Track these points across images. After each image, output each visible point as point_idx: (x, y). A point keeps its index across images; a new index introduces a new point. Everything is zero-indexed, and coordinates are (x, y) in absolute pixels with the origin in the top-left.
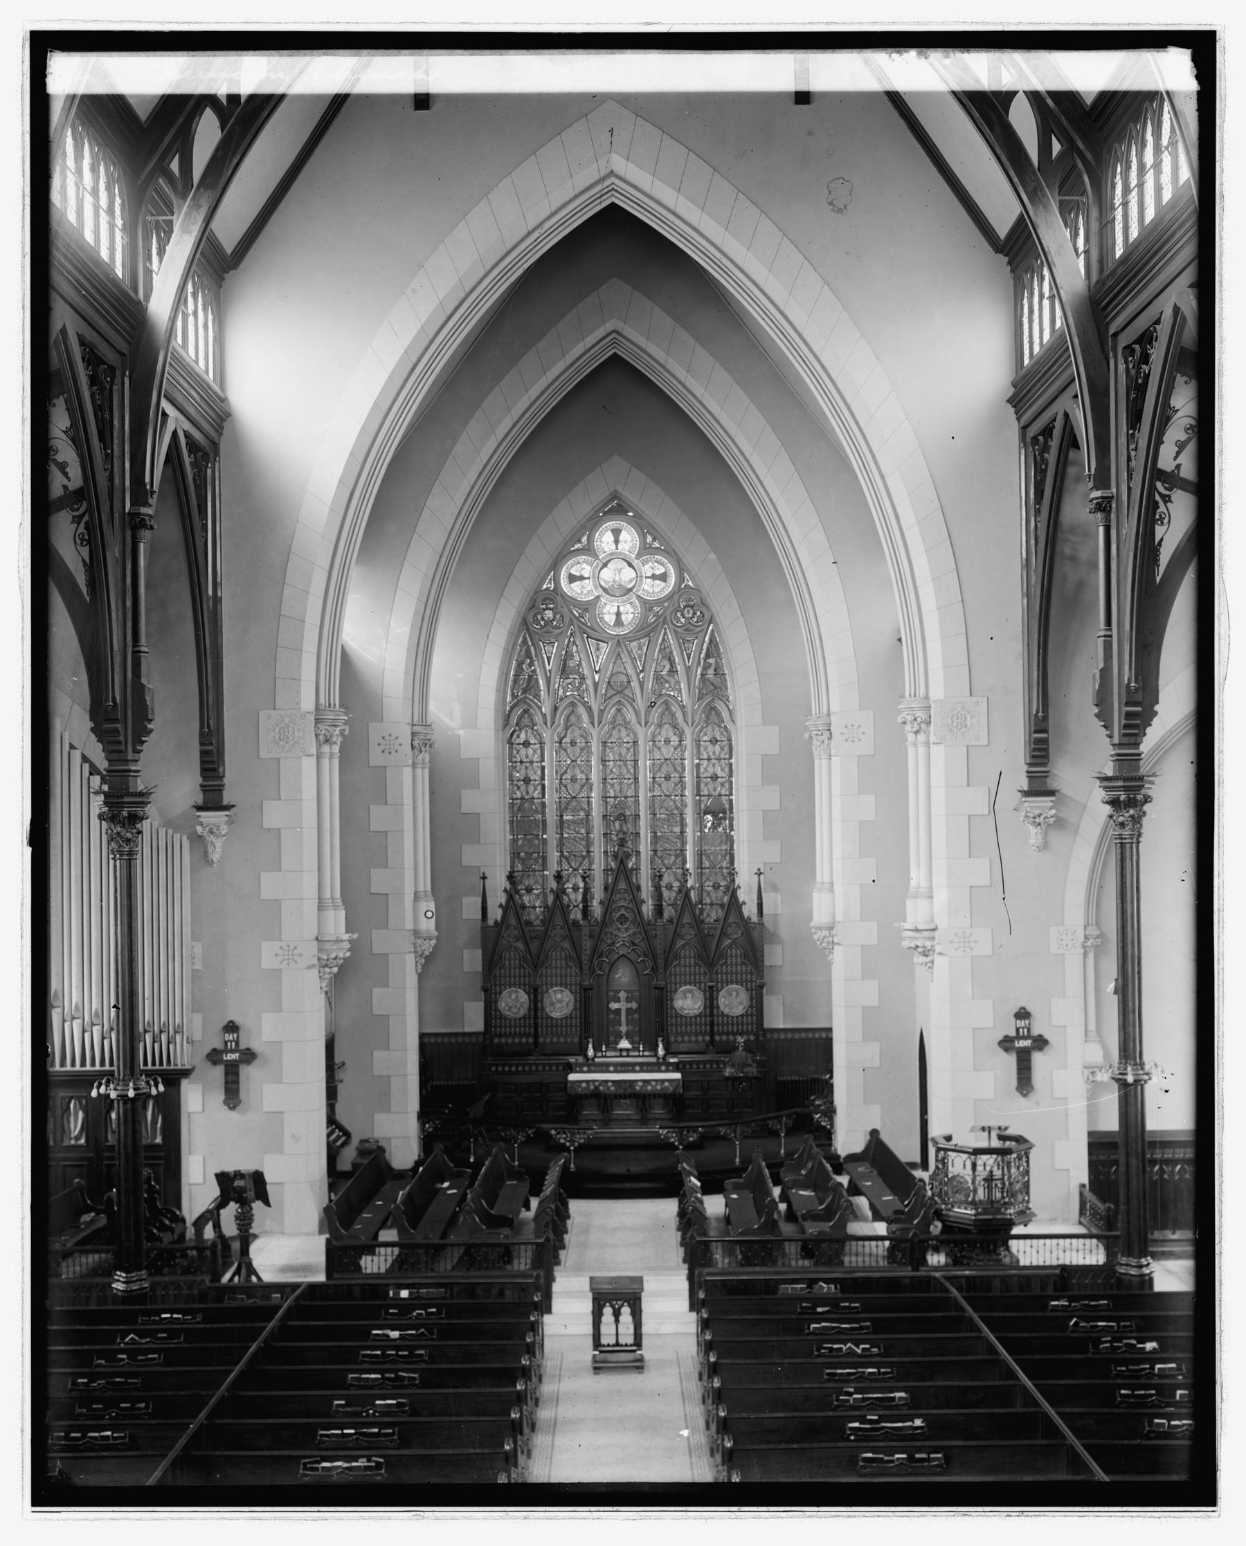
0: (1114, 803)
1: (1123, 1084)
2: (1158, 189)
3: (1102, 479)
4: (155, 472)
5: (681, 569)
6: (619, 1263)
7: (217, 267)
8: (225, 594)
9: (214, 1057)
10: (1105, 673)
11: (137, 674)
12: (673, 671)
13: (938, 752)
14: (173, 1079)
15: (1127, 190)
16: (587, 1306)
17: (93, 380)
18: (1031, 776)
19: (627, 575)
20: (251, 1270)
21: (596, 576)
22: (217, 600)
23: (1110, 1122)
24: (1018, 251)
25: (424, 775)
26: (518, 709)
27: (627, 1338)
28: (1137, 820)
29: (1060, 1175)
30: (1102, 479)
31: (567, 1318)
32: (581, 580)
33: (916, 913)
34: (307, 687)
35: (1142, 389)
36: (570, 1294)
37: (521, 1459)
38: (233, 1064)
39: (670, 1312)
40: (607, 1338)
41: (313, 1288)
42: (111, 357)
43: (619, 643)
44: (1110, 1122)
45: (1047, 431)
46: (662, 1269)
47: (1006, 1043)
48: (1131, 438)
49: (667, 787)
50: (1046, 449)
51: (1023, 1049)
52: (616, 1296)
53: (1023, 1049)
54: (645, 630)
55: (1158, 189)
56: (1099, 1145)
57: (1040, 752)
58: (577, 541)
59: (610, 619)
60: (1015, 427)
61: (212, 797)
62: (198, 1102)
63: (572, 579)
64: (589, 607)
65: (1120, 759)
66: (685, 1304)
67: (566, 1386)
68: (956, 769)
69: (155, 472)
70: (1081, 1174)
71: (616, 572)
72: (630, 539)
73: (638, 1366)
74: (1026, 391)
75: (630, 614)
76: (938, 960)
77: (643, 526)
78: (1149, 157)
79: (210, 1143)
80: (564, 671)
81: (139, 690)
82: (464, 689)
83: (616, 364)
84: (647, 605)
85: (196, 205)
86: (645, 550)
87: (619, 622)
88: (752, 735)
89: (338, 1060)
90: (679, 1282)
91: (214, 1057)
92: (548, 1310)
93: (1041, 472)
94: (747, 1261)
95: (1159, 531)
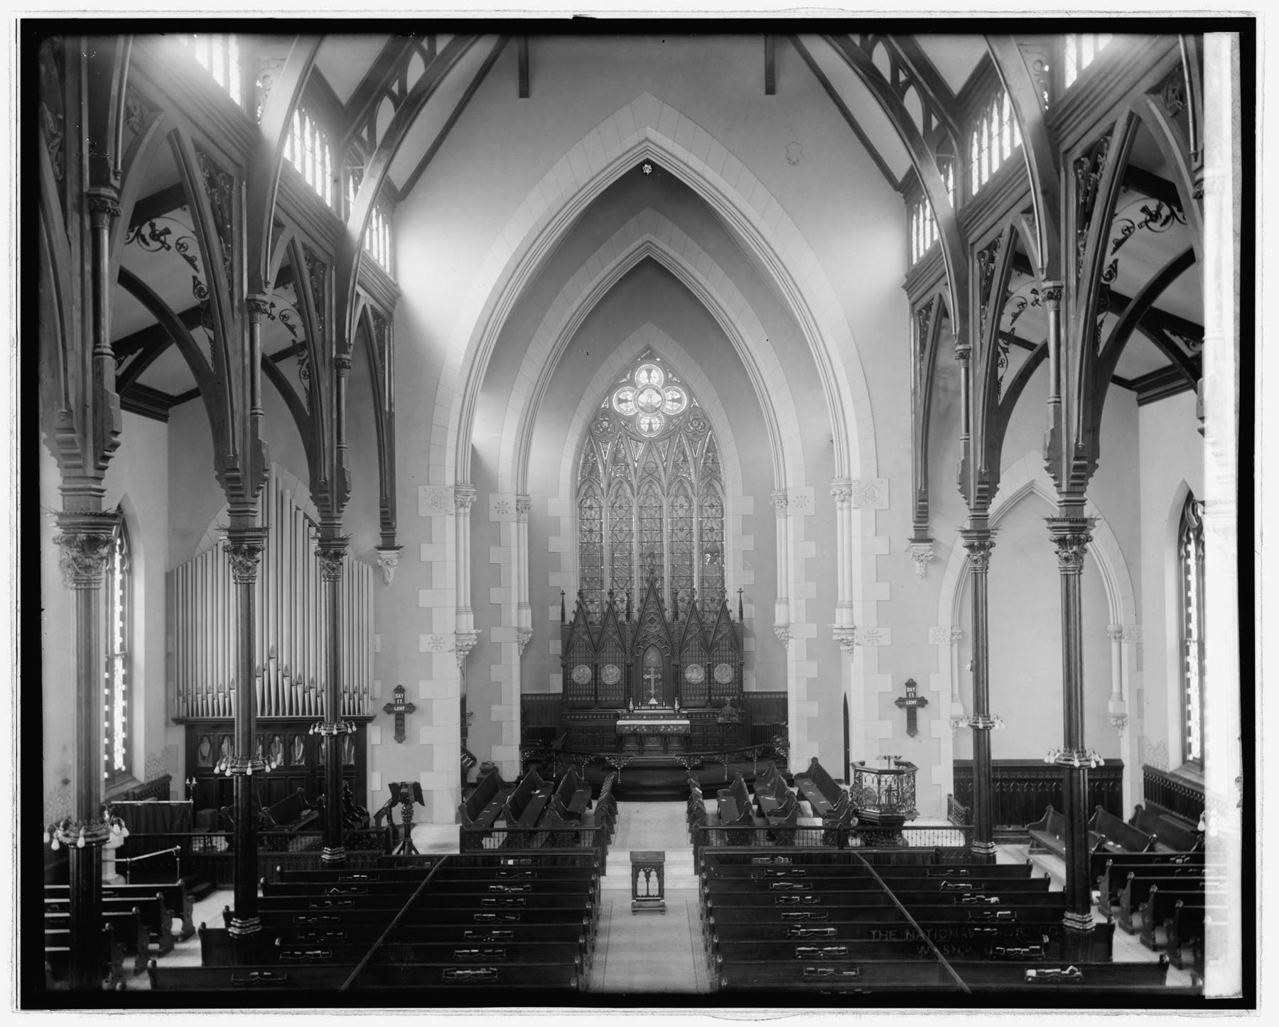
2: (1001, 149)
3: (963, 337)
4: (352, 333)
5: (691, 394)
6: (650, 843)
7: (393, 200)
8: (397, 410)
9: (389, 709)
11: (340, 462)
12: (685, 461)
13: (856, 514)
14: (363, 723)
15: (980, 150)
17: (312, 273)
18: (917, 530)
19: (656, 399)
20: (412, 847)
21: (635, 399)
22: (391, 414)
23: (968, 754)
25: (524, 528)
28: (985, 558)
31: (616, 878)
32: (625, 402)
34: (449, 470)
35: (990, 279)
36: (617, 863)
37: (586, 970)
38: (401, 713)
39: (682, 875)
43: (651, 444)
44: (968, 754)
45: (928, 307)
46: (677, 847)
47: (900, 702)
48: (982, 311)
50: (927, 317)
51: (912, 706)
52: (649, 864)
53: (912, 706)
55: (1001, 149)
56: (961, 769)
57: (922, 514)
58: (623, 377)
59: (645, 427)
61: (388, 542)
62: (377, 736)
63: (620, 401)
64: (631, 420)
66: (691, 870)
68: (868, 532)
69: (352, 333)
71: (650, 395)
72: (657, 376)
73: (662, 910)
74: (916, 279)
76: (856, 648)
77: (665, 366)
80: (615, 460)
82: (553, 462)
83: (649, 262)
84: (669, 419)
86: (668, 383)
87: (650, 430)
88: (736, 503)
90: (688, 856)
91: (389, 709)
92: (604, 874)
93: (924, 333)
95: (1001, 371)
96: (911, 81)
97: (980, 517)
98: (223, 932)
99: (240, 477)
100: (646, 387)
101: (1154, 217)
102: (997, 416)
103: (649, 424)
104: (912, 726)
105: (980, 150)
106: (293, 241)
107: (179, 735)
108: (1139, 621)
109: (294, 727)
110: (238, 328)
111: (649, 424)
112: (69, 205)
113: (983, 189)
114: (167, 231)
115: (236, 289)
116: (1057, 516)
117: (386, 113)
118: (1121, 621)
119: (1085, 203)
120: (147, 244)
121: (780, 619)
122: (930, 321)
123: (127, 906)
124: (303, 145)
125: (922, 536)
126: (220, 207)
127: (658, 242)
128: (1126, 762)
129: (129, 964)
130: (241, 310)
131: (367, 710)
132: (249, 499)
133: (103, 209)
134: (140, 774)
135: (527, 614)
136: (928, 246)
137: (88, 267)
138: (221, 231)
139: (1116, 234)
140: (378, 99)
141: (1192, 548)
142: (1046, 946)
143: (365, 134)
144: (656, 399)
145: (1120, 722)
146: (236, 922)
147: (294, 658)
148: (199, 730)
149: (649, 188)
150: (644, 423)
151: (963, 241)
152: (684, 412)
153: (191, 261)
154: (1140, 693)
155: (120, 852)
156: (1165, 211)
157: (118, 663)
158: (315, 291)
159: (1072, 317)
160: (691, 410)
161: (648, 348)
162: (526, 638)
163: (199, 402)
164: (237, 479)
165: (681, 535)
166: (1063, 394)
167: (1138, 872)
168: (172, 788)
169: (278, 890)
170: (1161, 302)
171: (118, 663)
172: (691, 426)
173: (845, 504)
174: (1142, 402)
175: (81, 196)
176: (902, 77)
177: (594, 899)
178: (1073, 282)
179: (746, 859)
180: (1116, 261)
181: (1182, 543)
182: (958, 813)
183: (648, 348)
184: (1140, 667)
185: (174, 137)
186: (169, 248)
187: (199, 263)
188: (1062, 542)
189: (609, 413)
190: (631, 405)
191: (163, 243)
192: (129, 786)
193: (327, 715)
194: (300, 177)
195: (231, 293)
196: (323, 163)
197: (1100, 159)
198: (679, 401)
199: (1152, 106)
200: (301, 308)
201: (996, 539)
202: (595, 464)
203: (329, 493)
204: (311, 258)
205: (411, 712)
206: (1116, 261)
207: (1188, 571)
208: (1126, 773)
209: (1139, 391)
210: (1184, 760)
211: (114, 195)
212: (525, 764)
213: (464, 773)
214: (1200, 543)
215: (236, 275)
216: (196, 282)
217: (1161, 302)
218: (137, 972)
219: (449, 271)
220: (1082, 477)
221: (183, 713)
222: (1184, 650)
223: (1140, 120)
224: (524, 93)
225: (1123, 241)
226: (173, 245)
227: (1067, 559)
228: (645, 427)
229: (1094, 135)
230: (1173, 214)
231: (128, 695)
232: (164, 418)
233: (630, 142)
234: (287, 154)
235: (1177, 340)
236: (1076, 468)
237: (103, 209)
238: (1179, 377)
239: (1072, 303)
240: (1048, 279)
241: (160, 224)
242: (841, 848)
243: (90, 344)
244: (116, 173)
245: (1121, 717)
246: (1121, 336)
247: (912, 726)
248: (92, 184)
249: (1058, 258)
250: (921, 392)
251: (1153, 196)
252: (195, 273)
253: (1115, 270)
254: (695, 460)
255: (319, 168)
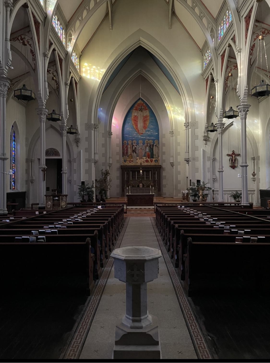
83: (140, 29)
120: (20, 41)
145: (254, 179)
173: (187, 128)
180: (255, 44)
186: (50, 74)
191: (49, 73)
205: (154, 173)
206: (255, 44)
212: (84, 10)
226: (51, 73)
242: (188, 201)
252: (31, 48)
253: (254, 46)
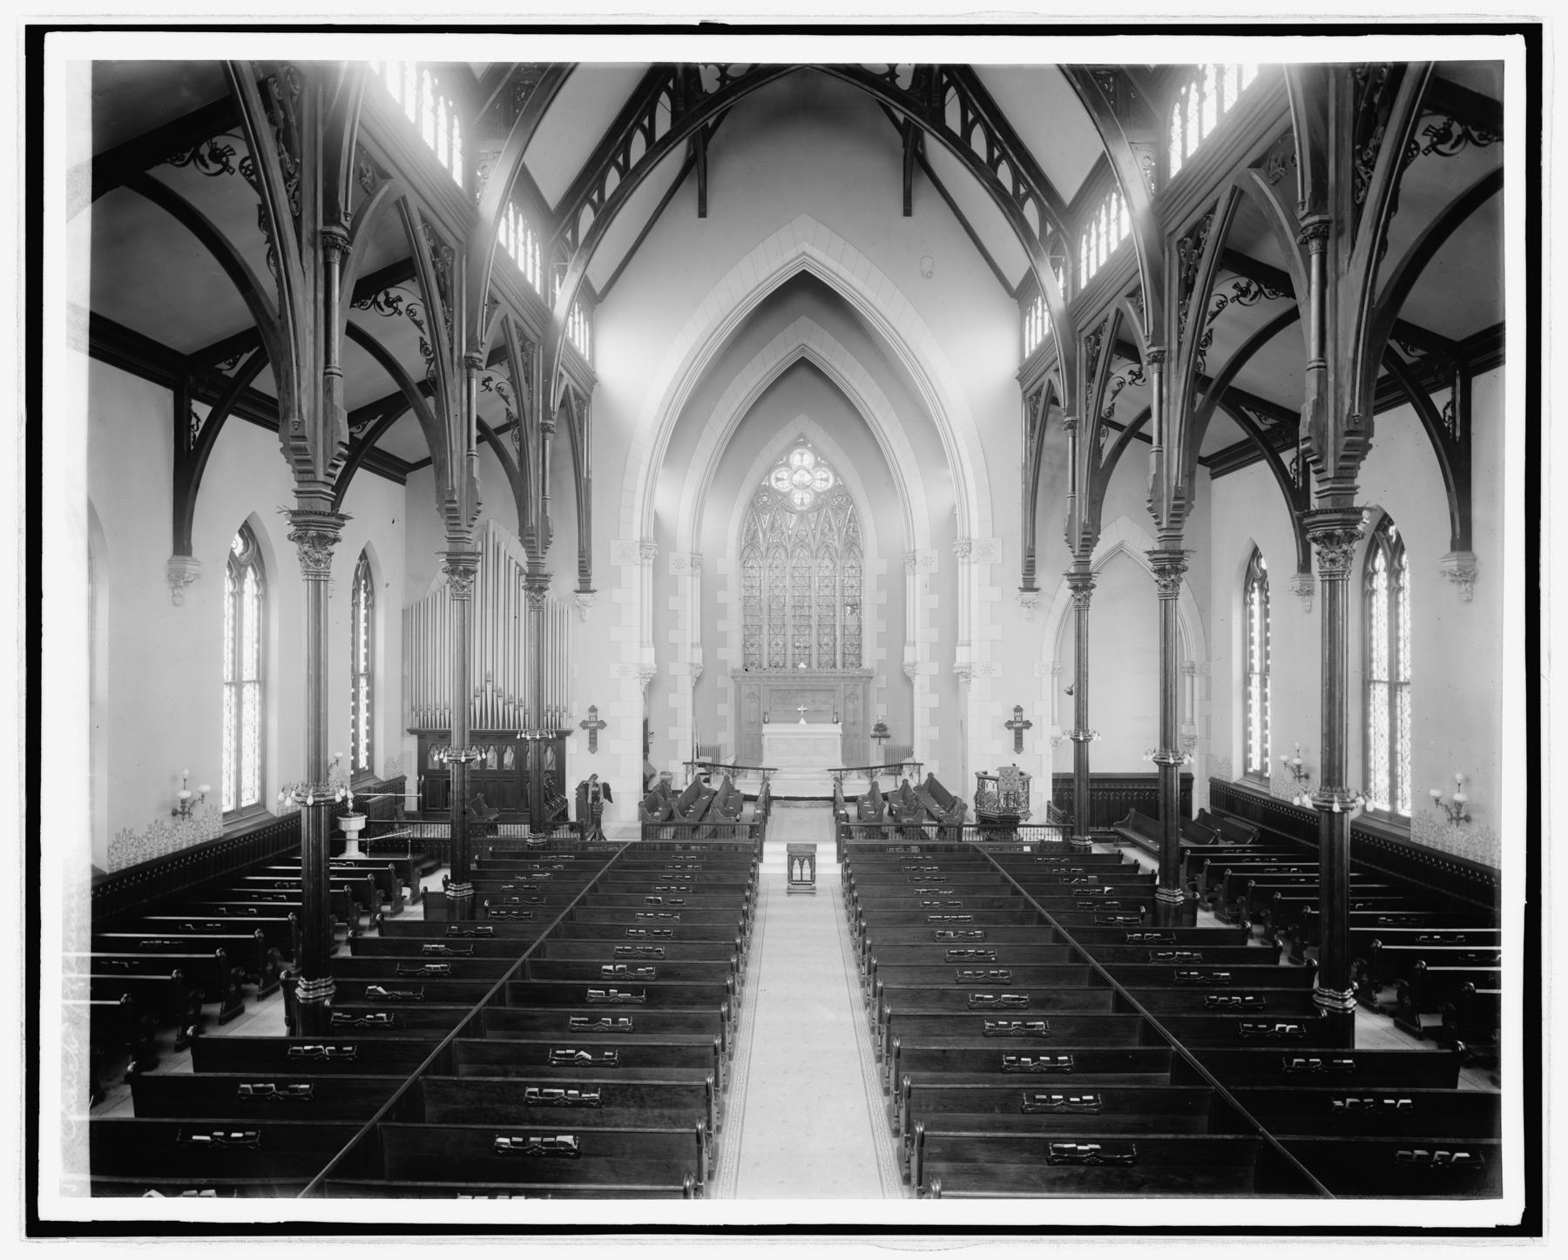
0: (1075, 588)
1: (1077, 742)
2: (1108, 245)
3: (1071, 410)
4: (555, 403)
5: (836, 474)
6: (802, 838)
7: (592, 299)
8: (593, 477)
9: (584, 725)
10: (1071, 517)
11: (544, 511)
12: (831, 529)
13: (974, 567)
14: (562, 735)
15: (1089, 250)
16: (785, 859)
17: (523, 349)
18: (1025, 580)
19: (807, 478)
20: (601, 836)
21: (791, 479)
22: (589, 480)
23: (1069, 768)
24: (1024, 293)
25: (697, 581)
26: (749, 544)
27: (807, 877)
28: (1087, 598)
29: (1041, 795)
30: (1071, 410)
31: (773, 863)
32: (782, 481)
33: (962, 656)
34: (636, 528)
35: (1095, 360)
36: (775, 853)
37: (741, 968)
38: (594, 728)
39: (828, 864)
40: (796, 877)
41: (634, 844)
42: (533, 337)
43: (802, 515)
44: (1069, 768)
45: (1038, 393)
46: (825, 841)
47: (1009, 725)
48: (1088, 387)
49: (827, 592)
50: (1038, 401)
51: (1018, 728)
52: (801, 855)
53: (1018, 728)
54: (816, 508)
55: (1108, 245)
56: (1060, 782)
57: (1030, 568)
58: (781, 460)
59: (798, 501)
60: (1020, 392)
61: (585, 587)
62: (575, 747)
63: (778, 480)
64: (786, 495)
65: (1078, 563)
66: (835, 858)
67: (770, 899)
68: (986, 583)
69: (555, 403)
70: (1049, 796)
71: (802, 474)
72: (808, 459)
73: (812, 892)
74: (1025, 373)
75: (808, 499)
76: (973, 680)
77: (816, 452)
78: (1103, 228)
79: (579, 768)
80: (772, 528)
81: (545, 519)
82: (723, 528)
83: (803, 363)
84: (818, 495)
85: (580, 257)
86: (817, 465)
87: (802, 504)
88: (874, 564)
89: (651, 729)
90: (833, 847)
91: (584, 725)
92: (761, 860)
93: (1034, 416)
94: (869, 837)
95: (1102, 440)
96: (1030, 193)
97: (1083, 561)
98: (442, 895)
99: (455, 513)
100: (800, 468)
101: (1244, 292)
102: (1099, 477)
103: (802, 499)
104: (1019, 744)
105: (1089, 250)
106: (506, 317)
107: (413, 742)
108: (1209, 659)
109: (503, 738)
110: (457, 380)
111: (802, 499)
112: (304, 239)
113: (1091, 282)
114: (399, 299)
115: (456, 347)
116: (1157, 548)
117: (587, 217)
118: (1194, 658)
119: (1187, 277)
121: (908, 659)
122: (1040, 404)
123: (364, 874)
124: (516, 238)
125: (1029, 586)
126: (443, 275)
127: (810, 345)
128: (1195, 774)
129: (365, 921)
130: (459, 365)
131: (565, 727)
132: (464, 527)
133: (335, 246)
134: (381, 774)
135: (699, 652)
136: (1040, 339)
137: (321, 296)
138: (443, 296)
139: (1213, 307)
140: (581, 206)
141: (1256, 596)
142: (1143, 916)
143: (569, 236)
144: (807, 478)
146: (452, 886)
147: (503, 677)
148: (429, 738)
149: (805, 291)
150: (797, 497)
151: (1073, 331)
152: (829, 490)
153: (419, 324)
154: (1208, 718)
155: (361, 833)
156: (1254, 288)
157: (363, 682)
158: (525, 365)
159: (1173, 376)
160: (836, 487)
161: (802, 435)
162: (698, 673)
163: (430, 469)
164: (454, 510)
165: (827, 592)
166: (1165, 444)
167: (1213, 859)
168: (407, 786)
169: (489, 865)
170: (1238, 381)
171: (363, 682)
172: (838, 502)
174: (1214, 476)
175: (315, 233)
176: (1022, 190)
177: (755, 876)
178: (1175, 346)
179: (882, 849)
181: (1247, 590)
182: (1055, 814)
183: (802, 435)
184: (1208, 697)
185: (401, 205)
187: (425, 327)
188: (1161, 572)
189: (768, 490)
190: (786, 483)
192: (370, 783)
193: (534, 725)
194: (512, 264)
195: (452, 350)
196: (533, 257)
197: (1202, 235)
198: (827, 480)
199: (1256, 177)
200: (513, 381)
201: (1096, 581)
202: (756, 531)
203: (534, 537)
204: (523, 338)
207: (1251, 616)
208: (1196, 784)
209: (1212, 467)
210: (1246, 773)
211: (344, 233)
213: (646, 784)
214: (1264, 589)
215: (456, 334)
216: (423, 345)
217: (1238, 381)
218: (371, 928)
219: (640, 356)
220: (1181, 506)
221: (416, 726)
222: (1247, 680)
223: (1242, 192)
224: (702, 213)
225: (1217, 313)
227: (1165, 586)
228: (798, 501)
229: (1198, 215)
230: (1260, 290)
231: (370, 708)
232: (403, 482)
233: (791, 254)
234: (502, 238)
235: (1251, 415)
236: (1175, 506)
237: (335, 246)
238: (1255, 448)
239: (1173, 365)
240: (1153, 345)
241: (393, 292)
243: (321, 364)
244: (346, 215)
245: (1193, 738)
246: (1207, 412)
247: (1019, 744)
248: (325, 223)
249: (1162, 327)
250: (1030, 465)
251: (1243, 275)
254: (839, 529)
255: (530, 260)
